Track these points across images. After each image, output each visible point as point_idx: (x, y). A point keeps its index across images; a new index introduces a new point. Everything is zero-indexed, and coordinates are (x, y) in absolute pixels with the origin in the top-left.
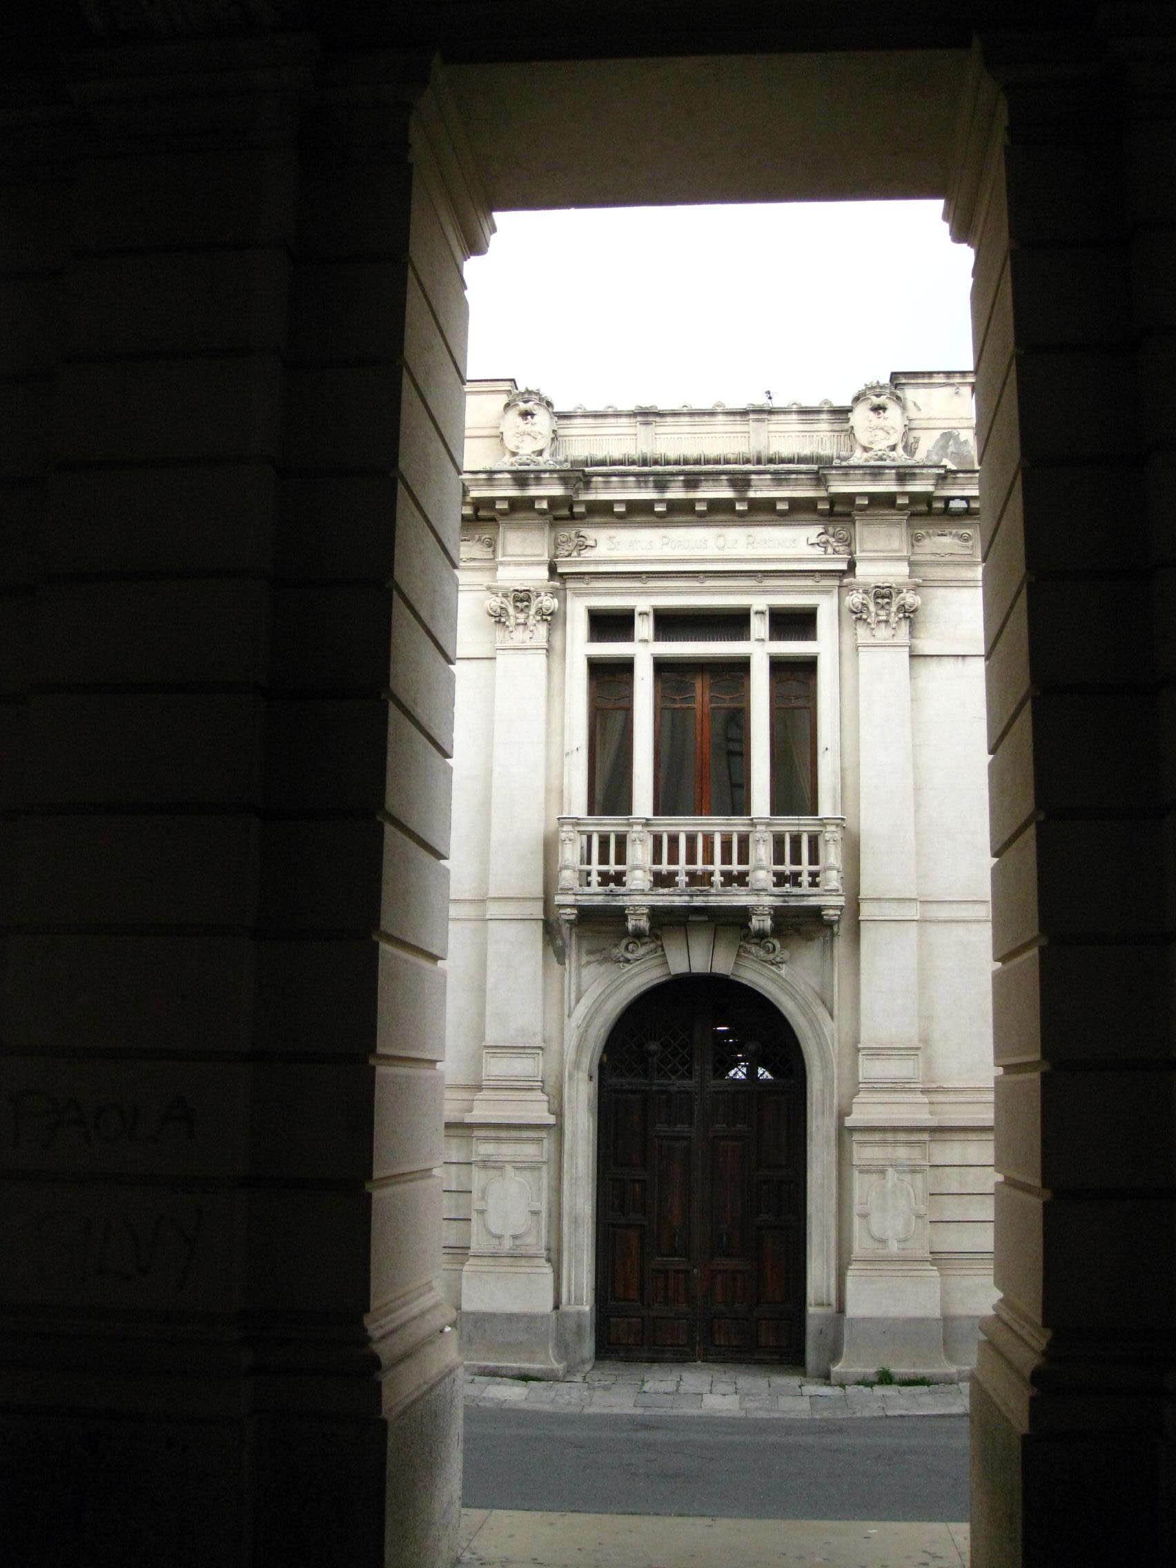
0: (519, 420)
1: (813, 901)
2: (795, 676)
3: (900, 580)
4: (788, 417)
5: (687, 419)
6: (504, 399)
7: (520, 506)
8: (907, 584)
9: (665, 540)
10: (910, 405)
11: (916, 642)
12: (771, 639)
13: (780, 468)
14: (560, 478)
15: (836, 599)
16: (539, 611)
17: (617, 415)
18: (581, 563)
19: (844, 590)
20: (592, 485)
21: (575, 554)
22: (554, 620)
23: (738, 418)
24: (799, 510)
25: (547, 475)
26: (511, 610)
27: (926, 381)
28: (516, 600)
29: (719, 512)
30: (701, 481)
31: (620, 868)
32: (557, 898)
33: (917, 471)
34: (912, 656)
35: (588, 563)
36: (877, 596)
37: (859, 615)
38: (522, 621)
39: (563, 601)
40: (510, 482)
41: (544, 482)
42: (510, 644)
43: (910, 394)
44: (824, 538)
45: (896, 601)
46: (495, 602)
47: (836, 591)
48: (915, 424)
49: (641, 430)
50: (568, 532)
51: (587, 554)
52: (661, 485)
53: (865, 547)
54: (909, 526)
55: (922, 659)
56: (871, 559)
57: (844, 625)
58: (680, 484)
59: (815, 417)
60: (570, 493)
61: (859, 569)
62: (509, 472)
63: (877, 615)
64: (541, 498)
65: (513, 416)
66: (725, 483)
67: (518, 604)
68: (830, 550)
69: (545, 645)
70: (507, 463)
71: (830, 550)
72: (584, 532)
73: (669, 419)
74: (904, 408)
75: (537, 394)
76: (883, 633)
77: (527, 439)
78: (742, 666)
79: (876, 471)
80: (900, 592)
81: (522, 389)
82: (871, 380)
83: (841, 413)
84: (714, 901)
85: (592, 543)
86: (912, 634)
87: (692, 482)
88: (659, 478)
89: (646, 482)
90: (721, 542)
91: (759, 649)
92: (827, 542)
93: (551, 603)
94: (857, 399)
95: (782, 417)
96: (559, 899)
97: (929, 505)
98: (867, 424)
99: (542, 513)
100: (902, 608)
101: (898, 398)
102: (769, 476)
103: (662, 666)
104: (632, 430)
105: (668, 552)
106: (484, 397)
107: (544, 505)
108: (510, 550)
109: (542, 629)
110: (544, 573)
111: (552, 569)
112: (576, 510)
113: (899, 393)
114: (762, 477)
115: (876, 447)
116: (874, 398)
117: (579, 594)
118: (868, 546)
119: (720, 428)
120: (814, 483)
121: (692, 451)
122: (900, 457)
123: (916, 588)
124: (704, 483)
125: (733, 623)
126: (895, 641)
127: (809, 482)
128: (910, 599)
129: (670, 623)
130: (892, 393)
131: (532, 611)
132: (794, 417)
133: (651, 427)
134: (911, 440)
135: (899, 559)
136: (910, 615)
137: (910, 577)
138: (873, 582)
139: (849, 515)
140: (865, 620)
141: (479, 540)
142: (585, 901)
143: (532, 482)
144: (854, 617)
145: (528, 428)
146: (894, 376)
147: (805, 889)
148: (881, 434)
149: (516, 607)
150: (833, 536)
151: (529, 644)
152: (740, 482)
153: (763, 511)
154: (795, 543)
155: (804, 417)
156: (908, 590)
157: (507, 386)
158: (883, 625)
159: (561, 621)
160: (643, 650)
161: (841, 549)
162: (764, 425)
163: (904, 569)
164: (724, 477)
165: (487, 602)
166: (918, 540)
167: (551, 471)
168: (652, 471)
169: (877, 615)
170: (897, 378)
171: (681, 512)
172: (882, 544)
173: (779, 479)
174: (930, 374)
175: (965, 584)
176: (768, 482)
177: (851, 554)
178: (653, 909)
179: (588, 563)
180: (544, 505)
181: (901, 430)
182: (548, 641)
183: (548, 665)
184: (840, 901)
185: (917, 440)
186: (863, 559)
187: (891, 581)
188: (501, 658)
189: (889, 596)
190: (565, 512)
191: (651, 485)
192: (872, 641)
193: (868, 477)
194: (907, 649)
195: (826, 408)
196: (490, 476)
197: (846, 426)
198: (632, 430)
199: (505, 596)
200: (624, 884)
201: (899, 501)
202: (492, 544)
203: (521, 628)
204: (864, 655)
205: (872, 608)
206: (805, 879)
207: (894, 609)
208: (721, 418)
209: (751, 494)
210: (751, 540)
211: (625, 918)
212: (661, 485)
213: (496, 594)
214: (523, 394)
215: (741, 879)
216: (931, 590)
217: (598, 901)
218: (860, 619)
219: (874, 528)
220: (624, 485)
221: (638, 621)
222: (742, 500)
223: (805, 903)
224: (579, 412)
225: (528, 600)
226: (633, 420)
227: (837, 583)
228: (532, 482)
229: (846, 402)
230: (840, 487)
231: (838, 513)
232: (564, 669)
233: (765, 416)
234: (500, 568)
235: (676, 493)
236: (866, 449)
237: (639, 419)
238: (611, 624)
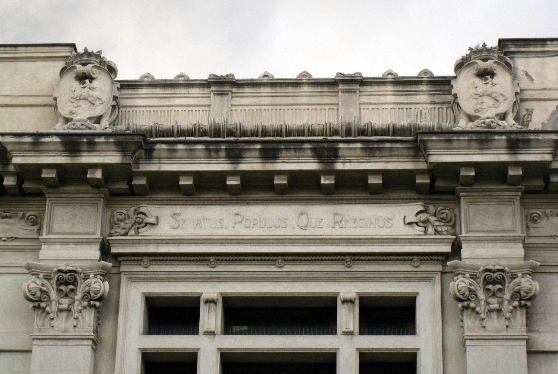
0: (76, 85)
3: (514, 263)
4: (382, 88)
5: (268, 90)
6: (61, 64)
7: (70, 178)
9: (238, 219)
10: (521, 74)
11: (534, 335)
12: (361, 333)
13: (372, 140)
14: (117, 143)
15: (438, 288)
16: (87, 296)
17: (189, 84)
18: (139, 242)
19: (447, 277)
20: (156, 154)
21: (132, 232)
22: (104, 307)
23: (326, 89)
24: (391, 187)
25: (102, 139)
26: (53, 295)
27: (538, 49)
28: (60, 282)
29: (302, 187)
30: (280, 150)
33: (532, 137)
34: (530, 353)
35: (149, 242)
36: (486, 282)
37: (465, 302)
38: (65, 306)
39: (116, 287)
40: (60, 147)
41: (98, 147)
42: (50, 333)
43: (521, 63)
44: (423, 217)
45: (509, 288)
46: (32, 283)
47: (438, 277)
48: (526, 95)
49: (215, 101)
50: (126, 210)
51: (146, 232)
52: (235, 155)
53: (472, 227)
54: (522, 205)
55: (542, 357)
56: (479, 240)
57: (448, 316)
58: (256, 154)
59: (413, 88)
60: (128, 160)
61: (466, 251)
62: (58, 135)
64: (94, 166)
65: (70, 83)
66: (309, 153)
67: (62, 288)
68: (430, 230)
69: (92, 335)
70: (60, 127)
71: (430, 230)
72: (145, 208)
73: (247, 90)
74: (514, 77)
75: (98, 55)
76: (495, 324)
77: (84, 105)
79: (484, 137)
80: (513, 277)
81: (80, 50)
82: (476, 42)
83: (442, 84)
85: (152, 220)
86: (529, 325)
87: (270, 153)
88: (231, 146)
89: (217, 151)
90: (303, 220)
92: (427, 221)
93: (101, 286)
94: (460, 66)
95: (376, 88)
97: (546, 180)
98: (472, 91)
99: (96, 184)
100: (516, 295)
101: (508, 64)
102: (359, 145)
104: (205, 101)
105: (242, 231)
106: (40, 64)
107: (98, 174)
108: (56, 227)
109: (89, 317)
110: (94, 252)
112: (135, 182)
113: (509, 60)
114: (351, 146)
115: (483, 115)
116: (480, 62)
117: (135, 279)
118: (476, 226)
119: (304, 100)
120: (411, 153)
122: (510, 124)
123: (534, 272)
124: (284, 153)
125: (318, 314)
126: (510, 332)
127: (405, 152)
128: (526, 283)
129: (241, 314)
130: (499, 58)
131: (79, 296)
132: (390, 88)
133: (226, 97)
134: (523, 112)
135: (514, 240)
136: (527, 303)
137: (525, 259)
138: (482, 264)
139: (453, 192)
140: (473, 309)
141: (23, 217)
143: (85, 147)
144: (460, 305)
145: (85, 92)
146: (503, 43)
148: (489, 102)
149: (59, 291)
150: (435, 215)
151: (72, 333)
153: (353, 187)
154: (390, 222)
155: (400, 88)
156: (524, 275)
157: (65, 52)
158: (494, 315)
159: (112, 309)
161: (445, 228)
162: (355, 97)
163: (518, 251)
164: (307, 146)
165: (25, 285)
166: (534, 221)
167: (107, 135)
168: (228, 141)
169: (487, 303)
170: (505, 46)
171: (257, 188)
172: (491, 224)
173: (370, 151)
174: (543, 41)
176: (359, 153)
177: (454, 234)
179: (149, 242)
180: (98, 174)
181: (512, 98)
182: (96, 332)
183: (95, 357)
185: (530, 112)
186: (469, 240)
188: (38, 351)
189: (502, 282)
190: (124, 186)
191: (223, 154)
192: (482, 333)
193: (474, 144)
194: (524, 343)
195: (425, 78)
196: (37, 140)
197: (450, 98)
198: (205, 101)
199: (48, 278)
201: (511, 173)
202: (37, 222)
203: (64, 315)
204: (474, 352)
205: (481, 295)
207: (507, 296)
208: (306, 89)
209: (339, 166)
210: (338, 218)
212: (235, 155)
213: (36, 275)
214: (81, 55)
216: (550, 277)
218: (467, 308)
219: (482, 206)
220: (191, 156)
221: (204, 310)
222: (327, 173)
224: (146, 81)
225: (74, 282)
226: (206, 91)
227: (439, 268)
228: (85, 147)
229: (450, 72)
230: (441, 156)
231: (440, 188)
232: (113, 366)
233: (356, 87)
234: (43, 247)
235: (251, 164)
236: (471, 118)
237: (213, 88)
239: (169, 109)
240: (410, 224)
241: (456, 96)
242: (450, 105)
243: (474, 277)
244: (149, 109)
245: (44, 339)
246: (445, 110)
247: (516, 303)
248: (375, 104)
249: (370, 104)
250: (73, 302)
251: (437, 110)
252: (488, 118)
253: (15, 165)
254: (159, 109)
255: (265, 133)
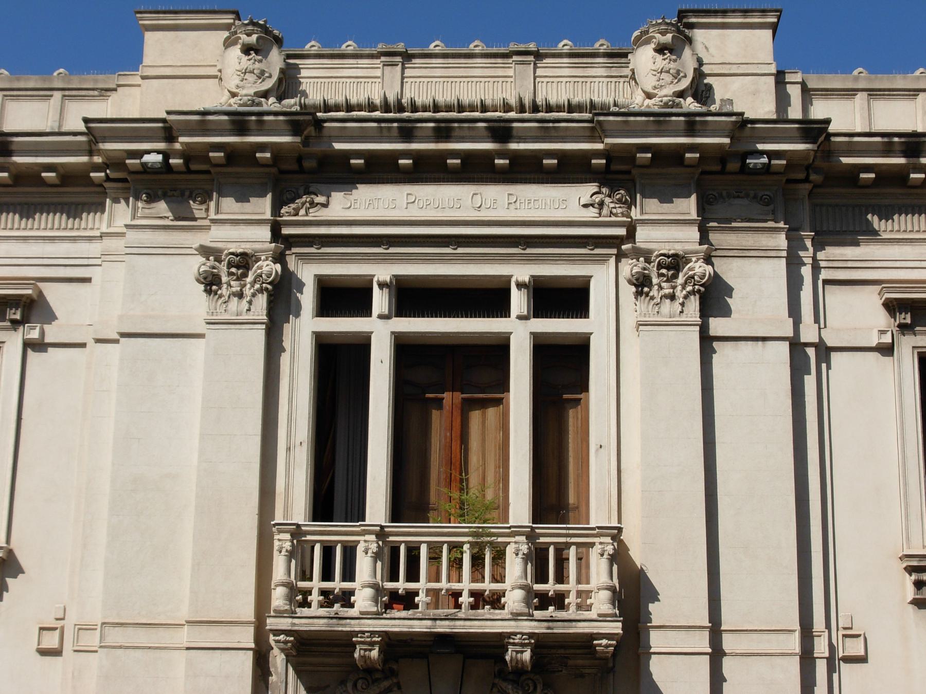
1: (583, 628)
2: (563, 370)
8: (697, 252)
12: (536, 316)
21: (302, 212)
24: (569, 170)
27: (719, 20)
29: (475, 170)
31: (347, 585)
32: (269, 621)
38: (667, 291)
44: (597, 198)
47: (612, 260)
61: (643, 235)
63: (661, 288)
71: (605, 211)
78: (498, 350)
84: (460, 627)
91: (519, 330)
96: (272, 623)
97: (301, 165)
103: (406, 350)
110: (265, 233)
111: (276, 234)
121: (445, 96)
125: (492, 298)
126: (683, 318)
129: (411, 297)
142: (302, 625)
147: (571, 613)
149: (230, 274)
151: (245, 317)
152: (501, 132)
153: (526, 170)
154: (566, 204)
160: (381, 330)
161: (619, 211)
166: (710, 204)
169: (661, 288)
171: (428, 170)
175: (765, 254)
178: (385, 635)
184: (616, 628)
186: (644, 222)
187: (678, 248)
190: (295, 167)
200: (352, 606)
206: (571, 600)
209: (513, 146)
211: (353, 646)
215: (496, 601)
217: (320, 625)
222: (502, 154)
223: (571, 631)
238: (343, 297)
239: (338, 80)
240: (585, 206)
241: (633, 71)
242: (627, 80)
243: (648, 261)
244: (316, 80)
245: (903, 438)
246: (621, 84)
247: (689, 288)
248: (594, 77)
249: (546, 77)
250: (245, 285)
251: (613, 84)
252: (666, 96)
253: (182, 143)
254: (327, 80)
255: (436, 108)
